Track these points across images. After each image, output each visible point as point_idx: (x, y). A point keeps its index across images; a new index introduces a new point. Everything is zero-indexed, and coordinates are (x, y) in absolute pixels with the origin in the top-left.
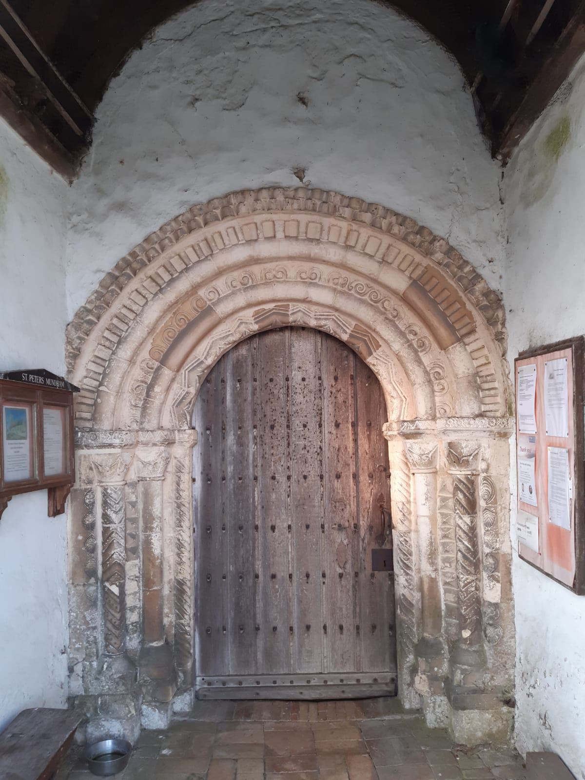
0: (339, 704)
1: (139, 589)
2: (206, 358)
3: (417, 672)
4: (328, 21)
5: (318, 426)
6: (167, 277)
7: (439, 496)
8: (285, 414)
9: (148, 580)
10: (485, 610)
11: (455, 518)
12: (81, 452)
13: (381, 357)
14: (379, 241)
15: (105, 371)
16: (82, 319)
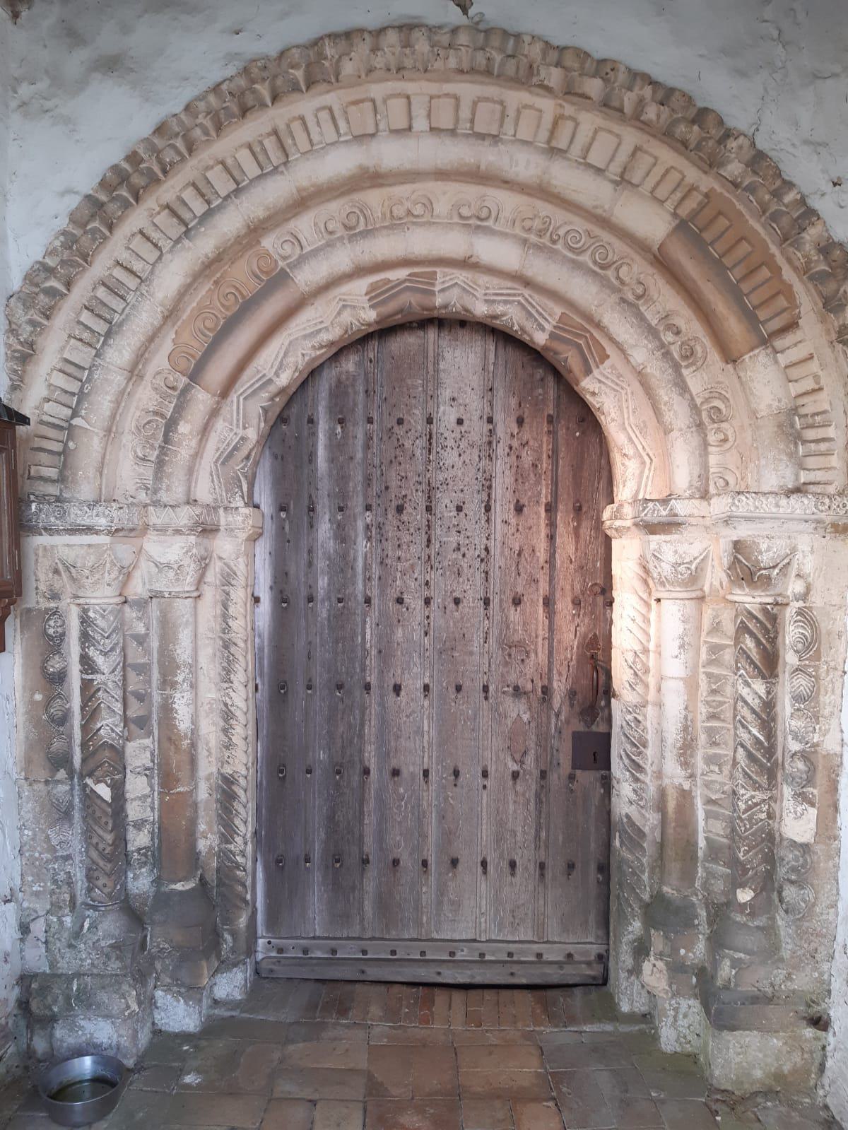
0: (505, 994)
1: (152, 790)
2: (277, 374)
3: (648, 955)
5: (483, 510)
7: (705, 642)
8: (424, 487)
10: (782, 853)
11: (734, 685)
13: (607, 378)
14: (616, 140)
16: (37, 285)
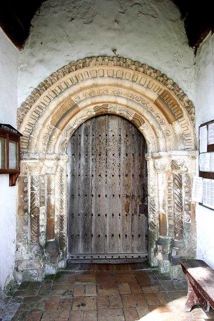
9: (48, 215)
12: (22, 162)
15: (32, 129)
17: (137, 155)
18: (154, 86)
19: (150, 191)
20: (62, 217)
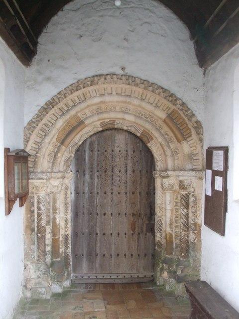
4: (137, 7)
6: (66, 109)
9: (54, 234)
15: (39, 147)
17: (144, 172)
18: (163, 104)
19: (157, 209)
20: (66, 236)
